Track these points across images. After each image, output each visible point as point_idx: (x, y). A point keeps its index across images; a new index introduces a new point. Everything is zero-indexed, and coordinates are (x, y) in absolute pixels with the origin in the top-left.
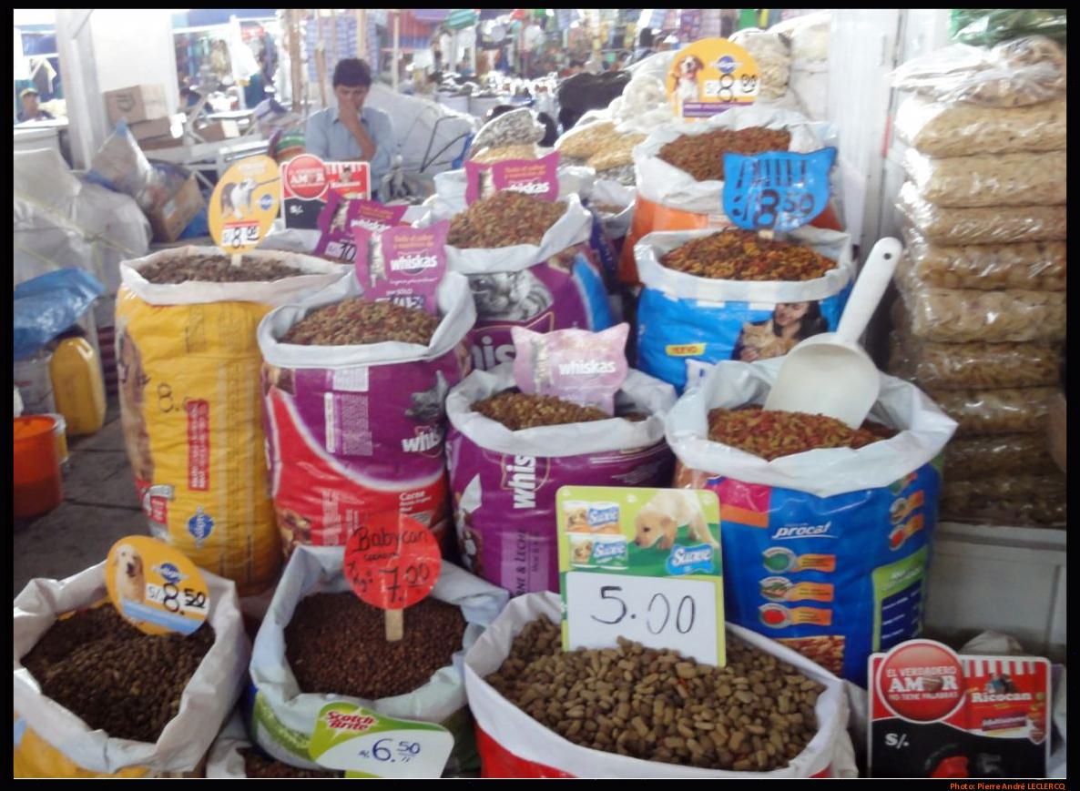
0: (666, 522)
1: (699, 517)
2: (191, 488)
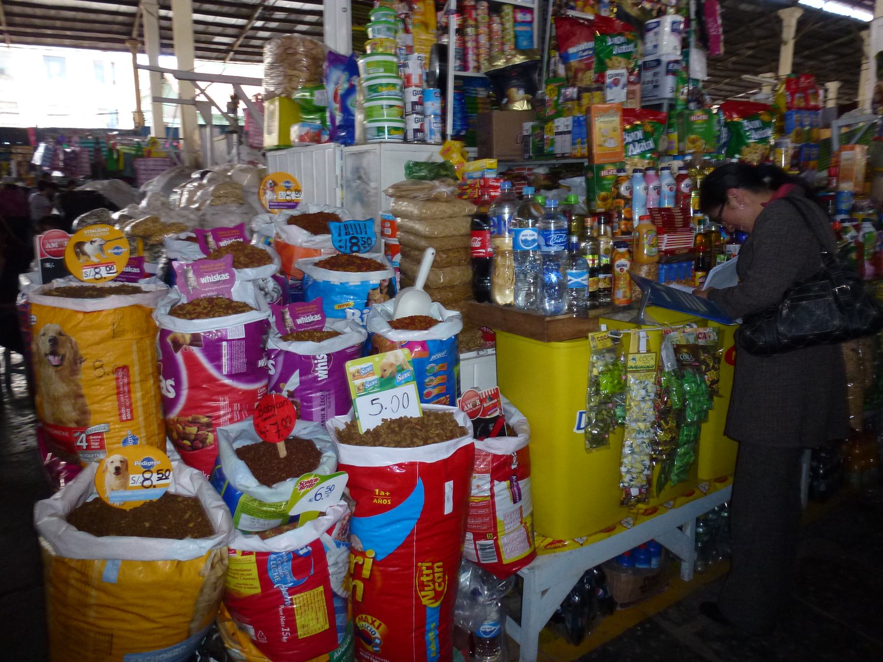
0: (392, 365)
1: (404, 360)
2: (122, 421)
